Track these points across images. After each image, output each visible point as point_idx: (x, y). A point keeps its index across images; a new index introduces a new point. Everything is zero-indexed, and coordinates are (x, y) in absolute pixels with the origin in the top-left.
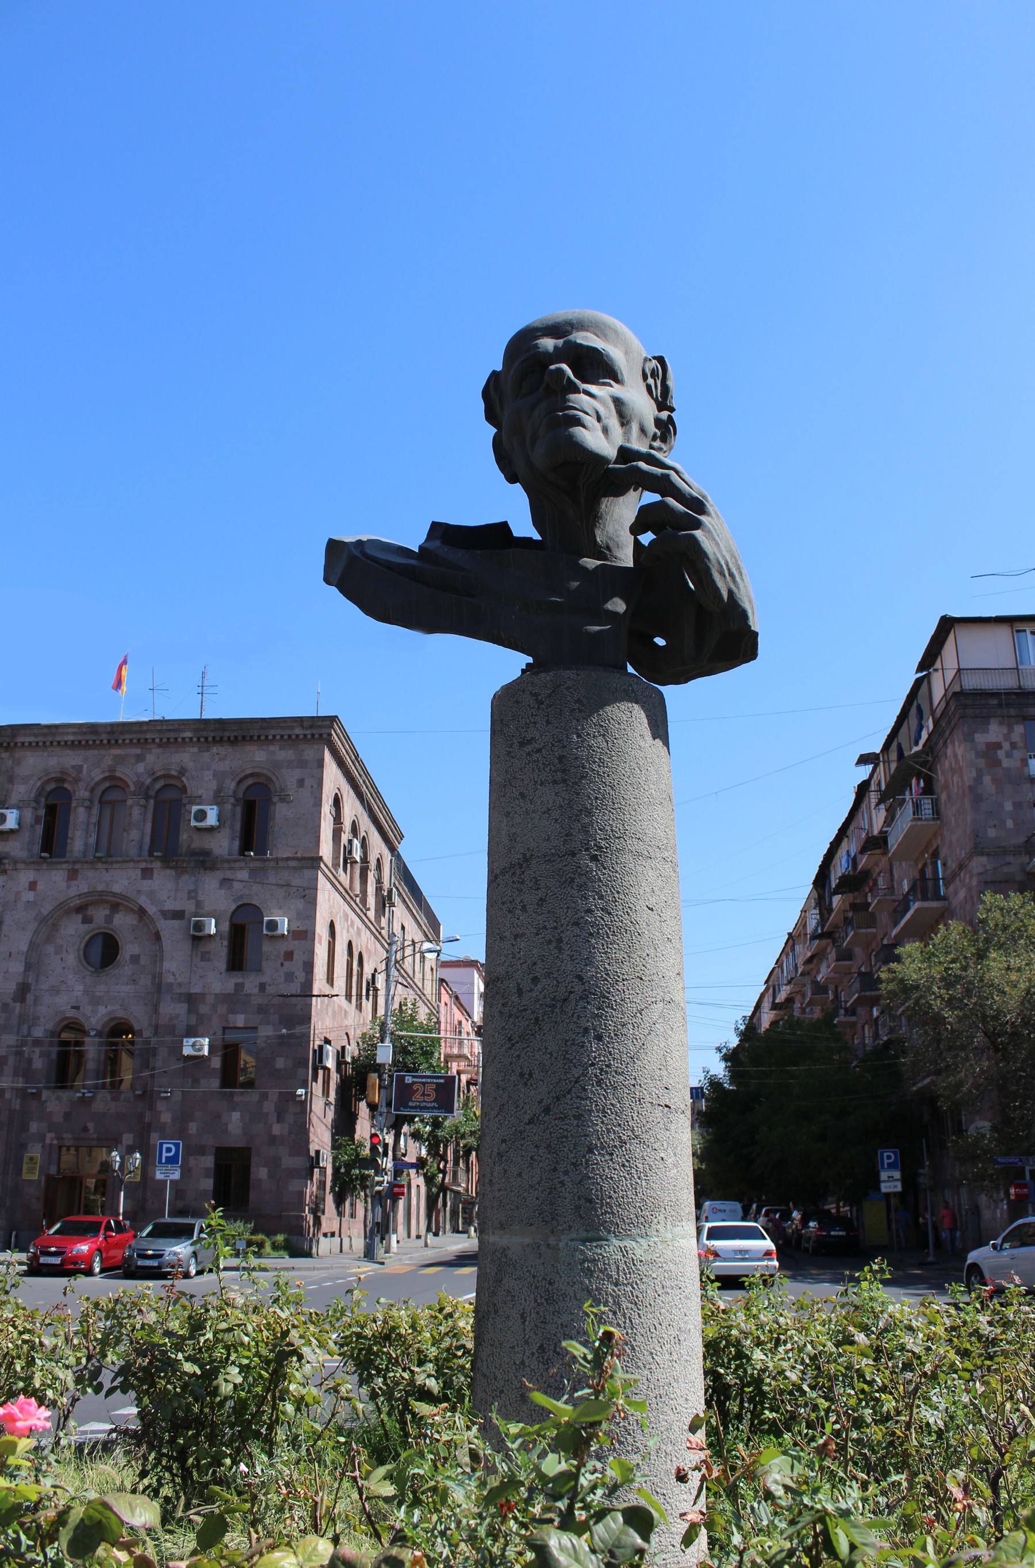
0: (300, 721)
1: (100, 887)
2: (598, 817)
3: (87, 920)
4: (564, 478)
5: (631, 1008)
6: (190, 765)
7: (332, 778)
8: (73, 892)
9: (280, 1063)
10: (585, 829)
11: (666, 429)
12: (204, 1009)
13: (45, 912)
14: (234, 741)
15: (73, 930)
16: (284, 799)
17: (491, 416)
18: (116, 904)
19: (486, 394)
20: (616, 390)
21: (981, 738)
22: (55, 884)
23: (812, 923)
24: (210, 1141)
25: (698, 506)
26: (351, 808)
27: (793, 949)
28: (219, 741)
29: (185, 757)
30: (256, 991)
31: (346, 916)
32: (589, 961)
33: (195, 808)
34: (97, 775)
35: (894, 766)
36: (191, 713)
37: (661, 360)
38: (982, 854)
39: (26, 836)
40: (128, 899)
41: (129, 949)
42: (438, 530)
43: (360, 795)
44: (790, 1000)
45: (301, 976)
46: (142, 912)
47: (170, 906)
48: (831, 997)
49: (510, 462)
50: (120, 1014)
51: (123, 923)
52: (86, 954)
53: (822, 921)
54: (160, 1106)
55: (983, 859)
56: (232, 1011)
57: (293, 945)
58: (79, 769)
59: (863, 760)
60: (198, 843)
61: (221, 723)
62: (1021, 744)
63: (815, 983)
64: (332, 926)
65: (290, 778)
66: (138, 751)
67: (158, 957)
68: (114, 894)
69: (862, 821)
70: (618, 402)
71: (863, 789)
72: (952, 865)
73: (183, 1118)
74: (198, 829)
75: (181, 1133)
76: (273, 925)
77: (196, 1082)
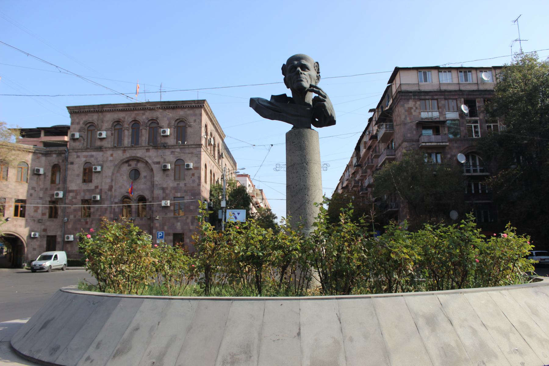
0: (194, 101)
1: (133, 155)
2: (307, 157)
3: (129, 165)
4: (300, 91)
5: (313, 190)
6: (160, 116)
7: (205, 119)
9: (192, 207)
10: (305, 159)
11: (318, 78)
12: (167, 192)
13: (116, 163)
14: (173, 108)
15: (126, 169)
16: (190, 126)
17: (283, 74)
18: (138, 160)
19: (282, 69)
20: (309, 72)
21: (406, 106)
22: (119, 155)
23: (355, 161)
24: (171, 232)
25: (325, 97)
26: (210, 127)
27: (348, 169)
28: (168, 108)
29: (158, 114)
30: (183, 185)
31: (210, 162)
32: (306, 182)
34: (130, 120)
35: (380, 113)
36: (159, 100)
37: (317, 63)
38: (405, 141)
39: (109, 139)
40: (142, 158)
41: (143, 174)
42: (273, 97)
43: (213, 124)
44: (347, 186)
45: (197, 181)
46: (147, 163)
47: (156, 160)
48: (360, 185)
49: (288, 82)
50: (141, 194)
51: (140, 166)
52: (130, 177)
53: (358, 161)
54: (155, 221)
55: (406, 143)
56: (177, 192)
57: (194, 171)
58: (124, 118)
59: (371, 111)
60: (163, 141)
62: (419, 108)
63: (355, 180)
64: (206, 165)
65: (191, 120)
66: (143, 112)
67: (152, 176)
68: (138, 157)
69: (370, 129)
70: (310, 75)
71: (370, 120)
72: (397, 145)
73: (163, 225)
74: (163, 136)
75: (163, 229)
76: (188, 165)
77: (166, 214)
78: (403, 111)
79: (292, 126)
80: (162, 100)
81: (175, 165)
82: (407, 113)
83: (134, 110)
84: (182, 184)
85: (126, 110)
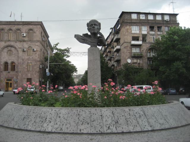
1: (9, 44)
6: (21, 27)
8: (6, 45)
18: (12, 46)
24: (26, 78)
33: (22, 34)
36: (20, 20)
46: (15, 48)
47: (20, 47)
49: (89, 30)
58: (5, 28)
61: (23, 22)
67: (18, 54)
78: (125, 30)
79: (90, 46)
80: (22, 21)
81: (28, 49)
82: (126, 31)
83: (10, 24)
84: (31, 57)
85: (6, 25)
